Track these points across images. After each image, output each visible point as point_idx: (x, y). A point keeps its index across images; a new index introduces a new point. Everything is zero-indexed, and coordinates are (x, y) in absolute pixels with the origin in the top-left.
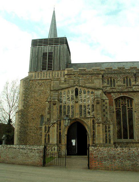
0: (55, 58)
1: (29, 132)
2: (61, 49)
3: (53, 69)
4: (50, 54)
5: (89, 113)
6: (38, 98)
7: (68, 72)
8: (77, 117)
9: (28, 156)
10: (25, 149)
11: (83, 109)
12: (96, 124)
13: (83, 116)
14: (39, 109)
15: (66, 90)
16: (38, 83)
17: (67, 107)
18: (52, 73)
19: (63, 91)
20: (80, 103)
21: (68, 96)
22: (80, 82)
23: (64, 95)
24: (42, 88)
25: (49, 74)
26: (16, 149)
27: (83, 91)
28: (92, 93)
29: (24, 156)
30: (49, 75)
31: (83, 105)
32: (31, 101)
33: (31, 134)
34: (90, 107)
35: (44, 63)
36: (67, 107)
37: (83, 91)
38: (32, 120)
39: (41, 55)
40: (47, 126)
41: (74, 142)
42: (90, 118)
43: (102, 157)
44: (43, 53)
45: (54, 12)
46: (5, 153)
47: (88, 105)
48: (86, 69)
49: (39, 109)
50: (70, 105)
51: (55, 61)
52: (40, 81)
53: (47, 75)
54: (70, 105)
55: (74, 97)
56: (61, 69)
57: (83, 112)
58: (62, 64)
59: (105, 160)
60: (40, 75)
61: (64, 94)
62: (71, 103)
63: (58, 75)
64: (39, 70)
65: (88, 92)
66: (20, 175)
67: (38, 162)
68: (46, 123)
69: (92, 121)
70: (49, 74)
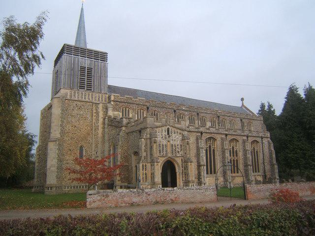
3: (92, 89)
4: (90, 70)
5: (178, 152)
6: (76, 124)
7: (115, 98)
8: (170, 155)
11: (174, 148)
15: (160, 129)
17: (161, 146)
18: (92, 95)
19: (157, 130)
20: (172, 142)
24: (82, 112)
25: (89, 95)
28: (180, 134)
30: (89, 96)
34: (179, 147)
35: (82, 80)
36: (161, 146)
39: (77, 69)
40: (144, 164)
45: (82, 9)
47: (178, 145)
51: (95, 80)
53: (85, 96)
55: (167, 136)
60: (77, 95)
62: (165, 142)
63: (99, 99)
70: (89, 95)
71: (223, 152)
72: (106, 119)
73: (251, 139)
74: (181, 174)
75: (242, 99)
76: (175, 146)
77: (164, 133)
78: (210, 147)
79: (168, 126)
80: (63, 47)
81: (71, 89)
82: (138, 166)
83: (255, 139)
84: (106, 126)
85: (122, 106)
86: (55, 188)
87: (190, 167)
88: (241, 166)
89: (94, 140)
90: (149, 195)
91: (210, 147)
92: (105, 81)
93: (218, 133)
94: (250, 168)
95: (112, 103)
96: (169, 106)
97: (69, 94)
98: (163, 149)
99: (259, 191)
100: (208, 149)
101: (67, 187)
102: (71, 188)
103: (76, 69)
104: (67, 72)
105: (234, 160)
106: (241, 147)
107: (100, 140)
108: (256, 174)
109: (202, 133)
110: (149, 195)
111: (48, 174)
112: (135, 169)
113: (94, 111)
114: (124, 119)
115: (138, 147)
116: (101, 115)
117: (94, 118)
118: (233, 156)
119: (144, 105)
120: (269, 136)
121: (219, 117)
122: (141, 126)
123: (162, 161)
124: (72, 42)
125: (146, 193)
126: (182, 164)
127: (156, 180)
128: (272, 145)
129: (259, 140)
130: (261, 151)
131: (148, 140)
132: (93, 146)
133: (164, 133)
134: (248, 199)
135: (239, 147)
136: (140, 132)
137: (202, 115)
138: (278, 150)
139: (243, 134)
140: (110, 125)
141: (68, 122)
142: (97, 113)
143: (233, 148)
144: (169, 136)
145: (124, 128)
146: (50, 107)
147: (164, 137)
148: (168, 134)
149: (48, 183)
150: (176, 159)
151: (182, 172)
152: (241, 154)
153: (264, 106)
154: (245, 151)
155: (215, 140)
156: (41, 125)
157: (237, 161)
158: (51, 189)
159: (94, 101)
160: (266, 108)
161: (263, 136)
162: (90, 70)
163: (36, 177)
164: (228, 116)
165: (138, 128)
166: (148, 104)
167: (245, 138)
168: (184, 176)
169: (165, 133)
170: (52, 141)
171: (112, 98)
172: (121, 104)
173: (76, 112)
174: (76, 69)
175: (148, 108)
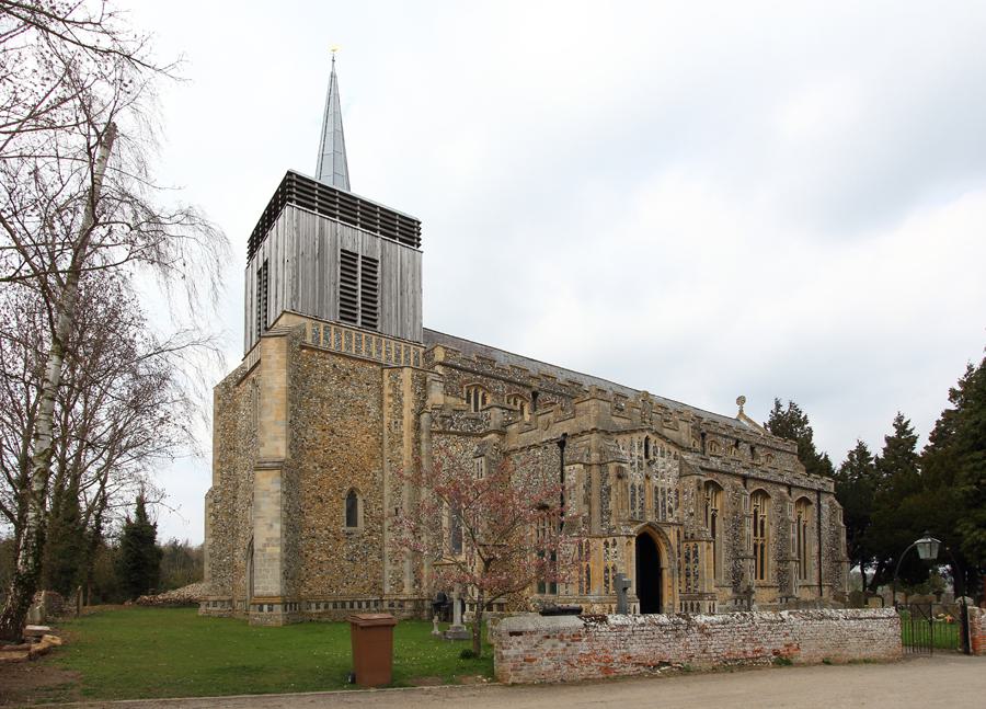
6: (336, 425)
8: (650, 518)
11: (660, 498)
15: (627, 438)
16: (335, 366)
19: (620, 439)
23: (624, 452)
24: (350, 391)
28: (675, 457)
32: (310, 431)
33: (316, 555)
34: (673, 495)
38: (318, 506)
42: (673, 524)
45: (333, 76)
47: (670, 491)
53: (359, 342)
55: (645, 461)
63: (398, 356)
66: (312, 702)
70: (369, 342)
73: (797, 495)
75: (741, 400)
76: (663, 493)
77: (636, 453)
79: (647, 433)
85: (467, 382)
90: (709, 635)
92: (414, 307)
93: (725, 473)
95: (439, 369)
97: (309, 333)
101: (314, 605)
102: (326, 607)
113: (388, 390)
116: (409, 400)
117: (387, 410)
119: (524, 386)
120: (832, 490)
121: (703, 435)
124: (309, 171)
125: (702, 629)
126: (678, 546)
129: (812, 497)
131: (595, 471)
132: (387, 490)
133: (636, 453)
134: (975, 653)
135: (767, 511)
136: (562, 444)
138: (849, 520)
139: (780, 479)
141: (312, 418)
142: (397, 396)
146: (242, 377)
150: (666, 530)
154: (784, 522)
158: (270, 610)
159: (383, 361)
162: (370, 263)
166: (535, 384)
167: (784, 490)
169: (638, 453)
172: (464, 377)
173: (331, 388)
175: (535, 395)
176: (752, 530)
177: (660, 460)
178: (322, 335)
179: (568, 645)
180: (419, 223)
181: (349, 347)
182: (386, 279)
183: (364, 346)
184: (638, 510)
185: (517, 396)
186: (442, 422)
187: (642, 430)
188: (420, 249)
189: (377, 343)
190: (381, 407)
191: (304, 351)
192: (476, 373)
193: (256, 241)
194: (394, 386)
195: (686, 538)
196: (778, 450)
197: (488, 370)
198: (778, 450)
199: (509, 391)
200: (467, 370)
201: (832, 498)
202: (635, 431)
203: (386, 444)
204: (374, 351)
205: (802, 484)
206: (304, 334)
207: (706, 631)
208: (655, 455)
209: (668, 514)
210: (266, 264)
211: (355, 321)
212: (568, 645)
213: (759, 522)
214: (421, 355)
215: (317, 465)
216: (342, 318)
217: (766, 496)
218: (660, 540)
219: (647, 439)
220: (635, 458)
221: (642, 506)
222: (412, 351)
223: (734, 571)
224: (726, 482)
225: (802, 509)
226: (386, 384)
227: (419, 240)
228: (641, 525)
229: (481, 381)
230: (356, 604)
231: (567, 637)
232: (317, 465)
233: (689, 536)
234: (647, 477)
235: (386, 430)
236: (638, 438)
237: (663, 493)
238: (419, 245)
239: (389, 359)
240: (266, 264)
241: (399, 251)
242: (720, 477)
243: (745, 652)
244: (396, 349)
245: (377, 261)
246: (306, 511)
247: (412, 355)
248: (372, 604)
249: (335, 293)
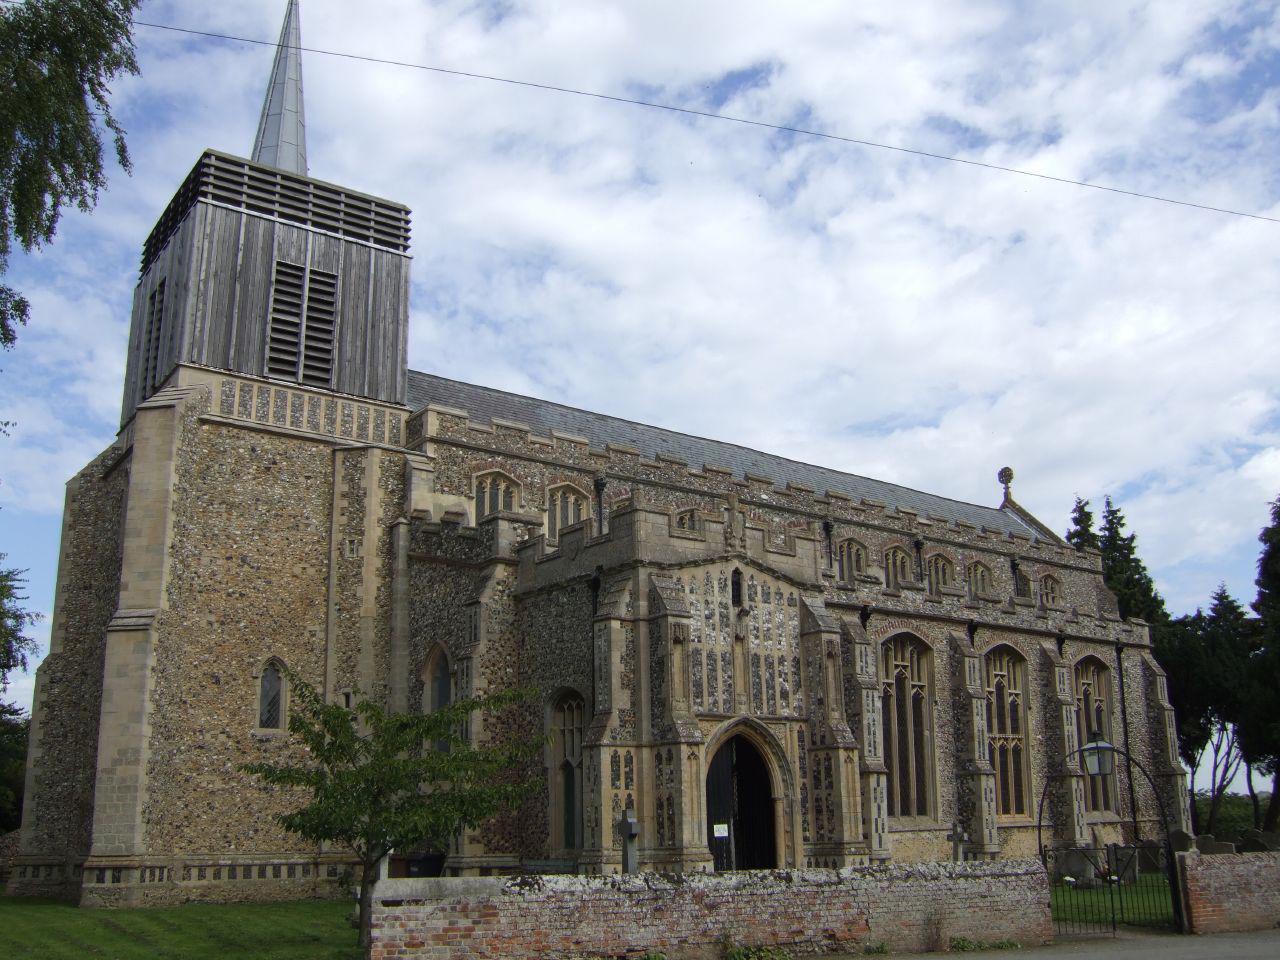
0: (350, 315)
1: (190, 764)
2: (384, 274)
3: (334, 381)
4: (324, 282)
6: (249, 549)
7: (443, 428)
8: (743, 711)
9: (994, 908)
10: (979, 877)
11: (764, 674)
12: (684, 748)
13: (765, 710)
14: (252, 622)
15: (700, 572)
16: (253, 450)
18: (331, 408)
19: (686, 575)
21: (707, 602)
22: (748, 542)
23: (693, 598)
24: (278, 490)
25: (314, 406)
26: (935, 878)
27: (759, 589)
28: (791, 602)
29: (981, 909)
30: (313, 413)
31: (762, 653)
32: (205, 560)
33: (203, 780)
34: (788, 667)
37: (759, 589)
38: (211, 690)
40: (622, 752)
41: (721, 830)
43: (1221, 888)
44: (279, 264)
46: (891, 905)
47: (782, 660)
48: (527, 432)
49: (252, 622)
50: (718, 651)
52: (265, 442)
53: (297, 409)
54: (718, 651)
55: (733, 611)
56: (383, 397)
57: (764, 689)
58: (384, 366)
59: (1229, 896)
61: (692, 592)
63: (363, 428)
64: (253, 364)
65: (776, 593)
67: (1039, 925)
68: (614, 738)
69: (795, 735)
70: (314, 406)
71: (961, 706)
72: (403, 529)
73: (1073, 653)
74: (798, 808)
75: (1006, 476)
76: (770, 665)
78: (900, 681)
79: (736, 563)
80: (200, 165)
81: (228, 369)
82: (674, 752)
83: (1090, 651)
84: (401, 564)
85: (478, 468)
86: (137, 874)
87: (843, 769)
88: (1036, 781)
89: (335, 631)
90: (712, 907)
91: (900, 681)
92: (395, 345)
94: (988, 784)
95: (431, 450)
96: (697, 484)
98: (712, 678)
99: (1245, 886)
100: (893, 691)
101: (195, 872)
102: (217, 876)
103: (259, 275)
104: (211, 284)
105: (1003, 751)
106: (1034, 687)
107: (369, 633)
108: (1097, 816)
109: (865, 613)
110: (712, 907)
111: (99, 799)
112: (560, 779)
113: (341, 487)
114: (503, 525)
115: (594, 670)
116: (376, 505)
117: (339, 520)
118: (1002, 730)
120: (1146, 641)
121: (918, 545)
122: (606, 558)
123: (713, 733)
124: (239, 145)
125: (699, 897)
126: (802, 759)
127: (686, 836)
128: (1162, 682)
129: (1106, 655)
130: (1118, 709)
131: (643, 628)
133: (717, 597)
135: (1025, 687)
136: (594, 585)
137: (847, 532)
139: (1040, 626)
140: (420, 560)
142: (357, 497)
143: (1000, 688)
144: (743, 613)
145: (500, 572)
147: (717, 617)
148: (737, 599)
149: (99, 846)
150: (774, 729)
151: (804, 801)
152: (1033, 720)
153: (1088, 516)
154: (1052, 708)
155: (922, 648)
156: (65, 556)
157: (1017, 751)
158: (116, 879)
159: (337, 437)
160: (1097, 526)
161: (1124, 638)
162: (324, 282)
163: (27, 817)
164: (962, 546)
165: (586, 565)
166: (601, 466)
167: (1050, 645)
168: (810, 817)
169: (721, 597)
170: (127, 629)
171: (432, 426)
172: (473, 459)
173: (245, 487)
174: (259, 275)
175: (599, 486)
176: (985, 722)
177: (762, 609)
178: (237, 399)
179: (475, 922)
180: (408, 212)
181: (279, 417)
182: (350, 304)
183: (306, 414)
184: (721, 697)
185: (567, 490)
186: (425, 541)
187: (726, 559)
188: (408, 253)
189: (328, 407)
190: (330, 515)
191: (205, 427)
192: (493, 453)
193: (156, 244)
194: (352, 480)
195: (814, 743)
196: (1065, 567)
197: (516, 447)
198: (1065, 567)
199: (553, 481)
200: (478, 449)
201: (1148, 656)
202: (712, 561)
203: (334, 580)
204: (322, 422)
205: (1085, 633)
206: (208, 400)
207: (707, 900)
208: (752, 599)
209: (779, 702)
210: (162, 285)
211: (294, 374)
212: (475, 922)
213: (1008, 707)
214: (403, 425)
215: (213, 618)
216: (272, 370)
217: (1017, 658)
218: (767, 749)
219: (737, 573)
220: (715, 607)
221: (729, 688)
222: (387, 418)
223: (959, 799)
224: (937, 637)
225: (1090, 679)
226: (339, 478)
227: (407, 239)
228: (726, 723)
229: (502, 466)
230: (269, 871)
231: (473, 910)
232: (213, 618)
233: (818, 739)
234: (738, 639)
235: (335, 554)
236: (721, 572)
237: (770, 665)
238: (406, 248)
239: (347, 433)
240: (162, 285)
241: (377, 256)
242: (925, 626)
243: (774, 934)
244: (360, 416)
245: (334, 277)
246: (190, 699)
247: (387, 424)
248: (299, 870)
249: (264, 330)
